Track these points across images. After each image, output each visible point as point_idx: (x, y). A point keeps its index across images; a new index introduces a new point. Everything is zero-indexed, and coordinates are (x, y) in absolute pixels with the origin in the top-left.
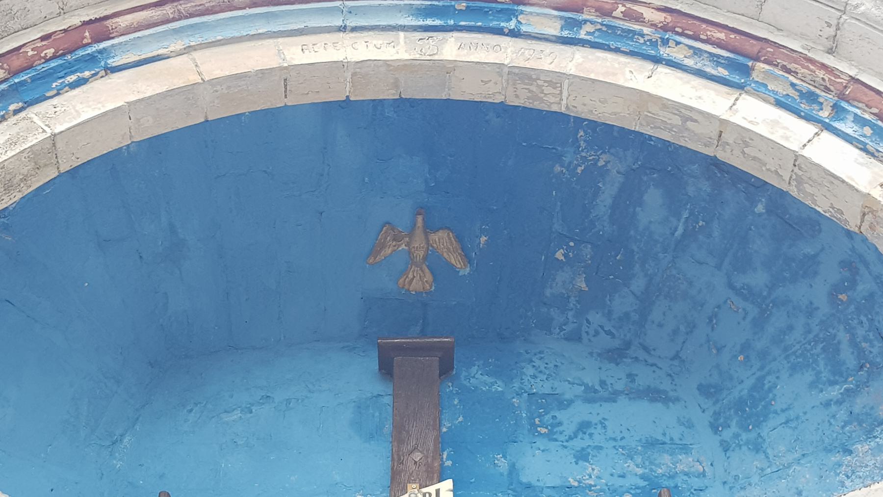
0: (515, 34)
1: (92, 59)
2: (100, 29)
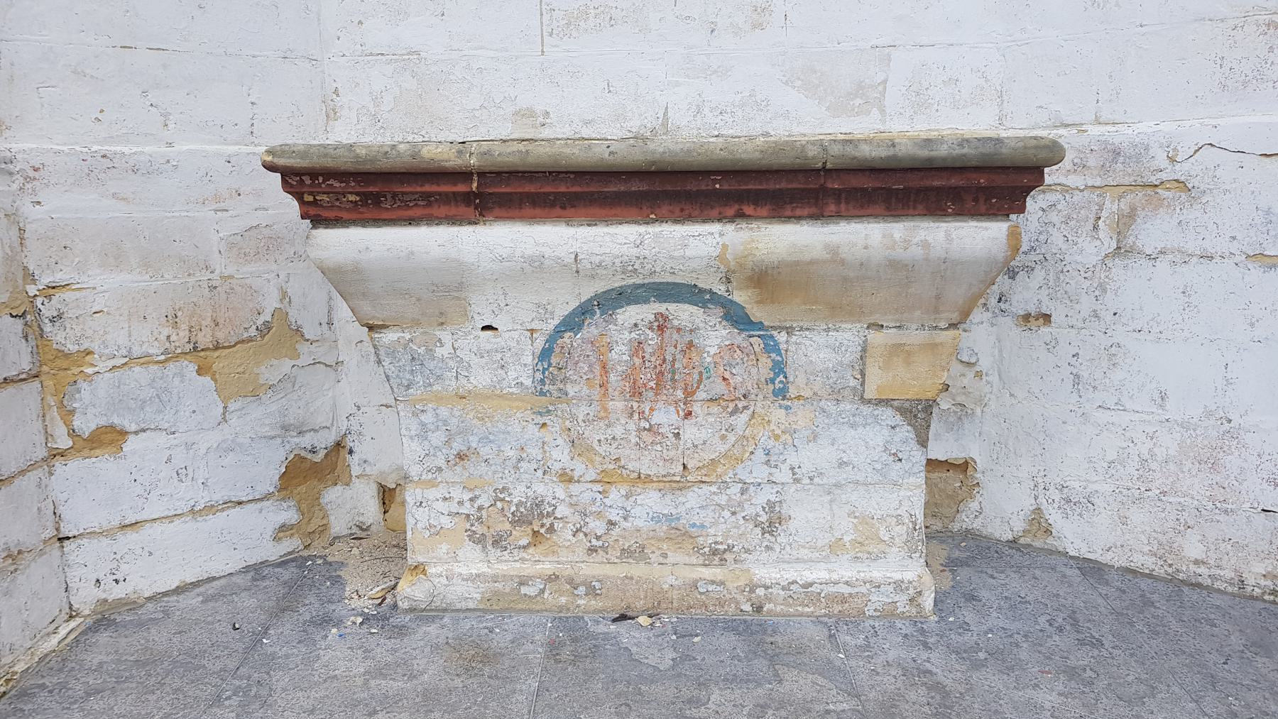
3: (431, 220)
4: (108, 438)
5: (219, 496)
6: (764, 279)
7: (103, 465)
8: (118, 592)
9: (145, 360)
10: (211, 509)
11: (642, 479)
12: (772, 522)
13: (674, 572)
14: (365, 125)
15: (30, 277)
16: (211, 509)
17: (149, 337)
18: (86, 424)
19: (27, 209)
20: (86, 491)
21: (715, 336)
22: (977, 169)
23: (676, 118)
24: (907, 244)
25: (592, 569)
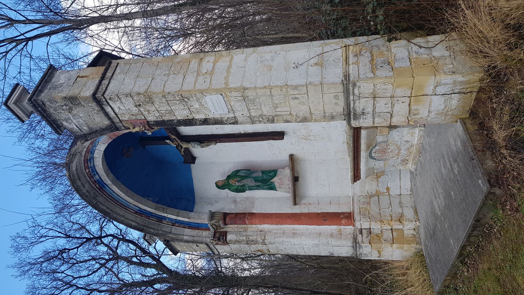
0: (100, 178)
1: (140, 211)
2: (136, 213)
3: (360, 173)
4: (388, 189)
5: (399, 176)
6: (368, 147)
7: (391, 190)
8: (409, 189)
9: (378, 184)
10: (400, 178)
11: (399, 152)
12: (408, 141)
13: (414, 150)
14: (349, 174)
15: (366, 195)
16: (400, 178)
17: (375, 183)
18: (386, 191)
19: (358, 195)
20: (395, 191)
21: (377, 148)
22: (354, 137)
23: (344, 129)
24: (364, 154)
25: (412, 156)
